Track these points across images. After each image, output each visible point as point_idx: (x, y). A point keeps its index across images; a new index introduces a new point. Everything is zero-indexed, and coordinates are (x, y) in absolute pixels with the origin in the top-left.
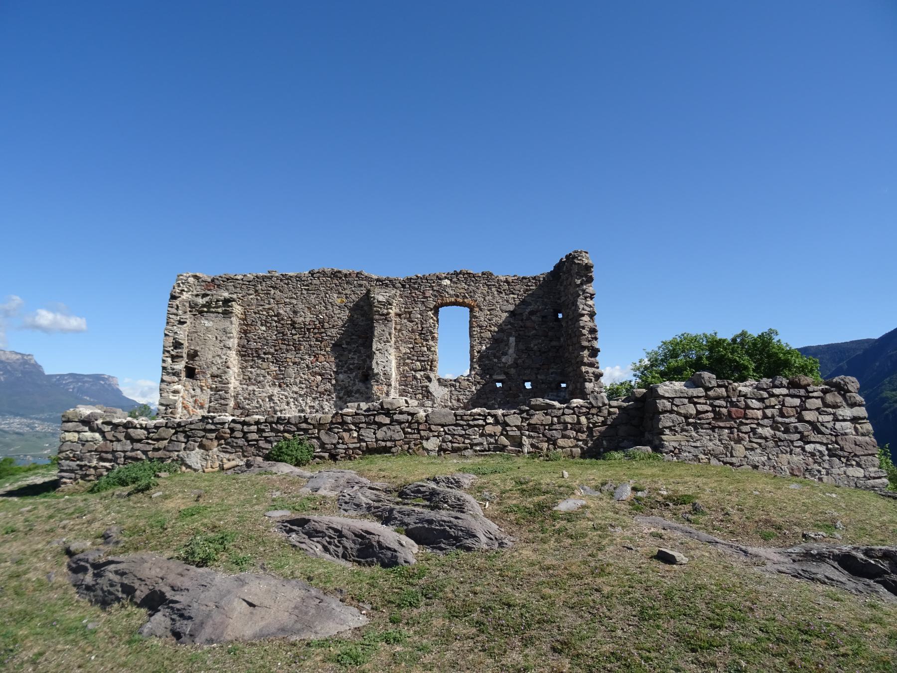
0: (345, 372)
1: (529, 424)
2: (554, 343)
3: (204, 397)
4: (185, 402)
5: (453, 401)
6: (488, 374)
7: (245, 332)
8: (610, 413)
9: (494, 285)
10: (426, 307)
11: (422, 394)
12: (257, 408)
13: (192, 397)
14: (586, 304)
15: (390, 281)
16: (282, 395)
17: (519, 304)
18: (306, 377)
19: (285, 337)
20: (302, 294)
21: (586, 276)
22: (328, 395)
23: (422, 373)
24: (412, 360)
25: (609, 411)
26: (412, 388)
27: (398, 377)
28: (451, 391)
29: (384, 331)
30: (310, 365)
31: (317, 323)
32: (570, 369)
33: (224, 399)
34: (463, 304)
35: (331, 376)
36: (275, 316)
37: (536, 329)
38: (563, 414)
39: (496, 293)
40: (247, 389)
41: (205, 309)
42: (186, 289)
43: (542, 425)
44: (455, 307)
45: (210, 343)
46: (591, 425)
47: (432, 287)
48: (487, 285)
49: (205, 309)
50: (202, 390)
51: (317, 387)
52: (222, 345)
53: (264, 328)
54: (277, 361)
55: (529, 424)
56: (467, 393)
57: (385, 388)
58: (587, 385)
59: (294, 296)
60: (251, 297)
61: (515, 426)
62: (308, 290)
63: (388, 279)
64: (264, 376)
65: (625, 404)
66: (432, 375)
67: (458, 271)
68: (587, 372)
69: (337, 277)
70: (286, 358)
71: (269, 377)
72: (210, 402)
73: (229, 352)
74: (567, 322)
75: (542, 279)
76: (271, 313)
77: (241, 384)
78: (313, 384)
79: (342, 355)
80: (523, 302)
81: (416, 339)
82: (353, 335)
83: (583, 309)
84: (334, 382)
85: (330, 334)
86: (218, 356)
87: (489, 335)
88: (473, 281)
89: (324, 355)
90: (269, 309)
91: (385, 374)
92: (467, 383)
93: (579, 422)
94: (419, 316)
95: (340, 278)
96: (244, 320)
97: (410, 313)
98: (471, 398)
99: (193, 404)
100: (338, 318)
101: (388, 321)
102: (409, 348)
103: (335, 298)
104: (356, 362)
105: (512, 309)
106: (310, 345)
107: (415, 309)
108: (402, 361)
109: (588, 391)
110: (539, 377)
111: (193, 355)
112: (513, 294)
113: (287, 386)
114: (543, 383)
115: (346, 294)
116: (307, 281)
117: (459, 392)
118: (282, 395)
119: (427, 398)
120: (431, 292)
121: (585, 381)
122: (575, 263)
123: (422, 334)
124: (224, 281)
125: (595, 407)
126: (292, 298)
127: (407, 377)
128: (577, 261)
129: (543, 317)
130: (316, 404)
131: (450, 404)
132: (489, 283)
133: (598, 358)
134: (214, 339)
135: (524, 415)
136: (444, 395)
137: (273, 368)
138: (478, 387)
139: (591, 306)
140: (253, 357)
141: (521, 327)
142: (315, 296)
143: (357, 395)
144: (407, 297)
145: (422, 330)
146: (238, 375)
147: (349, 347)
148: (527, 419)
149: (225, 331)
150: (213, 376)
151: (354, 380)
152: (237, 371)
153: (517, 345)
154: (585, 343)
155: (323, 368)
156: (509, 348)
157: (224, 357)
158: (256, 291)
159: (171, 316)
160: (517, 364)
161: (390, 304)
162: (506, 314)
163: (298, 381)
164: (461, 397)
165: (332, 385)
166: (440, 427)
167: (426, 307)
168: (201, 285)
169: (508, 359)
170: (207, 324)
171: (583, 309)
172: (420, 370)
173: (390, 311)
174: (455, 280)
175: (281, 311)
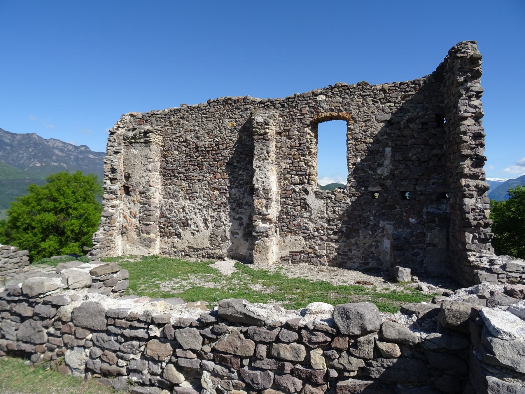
0: (237, 187)
1: (213, 350)
2: (435, 152)
3: (136, 209)
4: (125, 213)
5: (329, 213)
6: (363, 186)
7: (165, 157)
8: (378, 353)
9: (369, 95)
10: (303, 124)
11: (300, 206)
12: (175, 217)
13: (129, 209)
14: (469, 105)
15: (271, 102)
16: (191, 206)
17: (396, 113)
18: (207, 191)
19: (192, 159)
20: (202, 121)
21: (472, 71)
22: (224, 207)
23: (300, 186)
24: (292, 174)
25: (376, 348)
26: (292, 200)
27: (280, 191)
28: (327, 203)
29: (262, 149)
30: (210, 182)
31: (214, 145)
32: (451, 180)
33: (148, 211)
34: (338, 118)
35: (226, 191)
36: (184, 142)
37: (414, 138)
38: (278, 340)
39: (371, 103)
40: (168, 202)
41: (133, 141)
42: (121, 126)
43: (236, 356)
44: (330, 122)
45: (137, 167)
46: (334, 374)
47: (308, 104)
48: (362, 96)
49: (133, 141)
50: (134, 204)
51: (216, 200)
52: (145, 168)
53: (177, 153)
54: (187, 179)
55: (213, 350)
56: (342, 205)
57: (264, 202)
58: (467, 201)
59: (197, 124)
60: (168, 127)
61: (192, 350)
62: (206, 117)
63: (269, 101)
64: (179, 192)
65: (418, 336)
66: (309, 188)
67: (333, 86)
68: (468, 186)
69: (227, 103)
70: (193, 176)
71: (182, 192)
72: (140, 213)
73: (150, 173)
74: (449, 128)
75: (422, 82)
76: (182, 140)
77: (164, 198)
78: (213, 197)
79: (234, 172)
80: (401, 110)
81: (294, 155)
82: (242, 154)
83: (466, 111)
84: (228, 195)
85: (223, 154)
86: (143, 177)
87: (364, 147)
88: (347, 93)
89: (220, 173)
90: (180, 136)
91: (264, 189)
92: (342, 195)
93: (307, 362)
94: (297, 133)
95: (231, 104)
96: (164, 146)
97: (289, 130)
98: (347, 210)
99: (129, 214)
100: (230, 140)
101: (266, 140)
102: (289, 164)
103: (228, 123)
104: (245, 178)
105: (388, 118)
106: (210, 165)
107: (293, 126)
108: (282, 176)
109: (466, 209)
110: (418, 188)
111: (128, 177)
112: (390, 102)
113: (195, 199)
114: (422, 194)
115: (235, 118)
116: (206, 110)
117: (335, 204)
118: (191, 206)
119: (306, 210)
120: (307, 109)
121: (464, 196)
122: (458, 58)
123: (299, 149)
124: (149, 117)
125: (344, 336)
126: (195, 126)
127: (287, 190)
128: (459, 55)
129: (423, 124)
130: (215, 214)
131: (326, 215)
132: (364, 94)
133: (484, 169)
134: (140, 164)
135: (207, 331)
136: (320, 207)
137: (184, 185)
138: (354, 199)
139: (476, 107)
140: (171, 176)
141: (399, 136)
142: (212, 122)
143: (246, 207)
144: (286, 116)
145: (300, 146)
146: (162, 191)
147: (239, 165)
148: (211, 340)
149: (147, 157)
150: (141, 193)
151: (244, 194)
152: (160, 188)
153: (393, 156)
154: (466, 152)
155: (220, 184)
156: (385, 160)
157: (147, 178)
158: (171, 122)
159: (109, 148)
160: (393, 175)
161: (267, 124)
162: (382, 124)
163: (202, 195)
164: (336, 209)
165: (227, 198)
166: (88, 332)
167: (303, 124)
168: (135, 122)
169: (383, 171)
170: (136, 152)
171: (466, 111)
172: (299, 184)
173: (267, 130)
174: (330, 94)
175: (188, 138)
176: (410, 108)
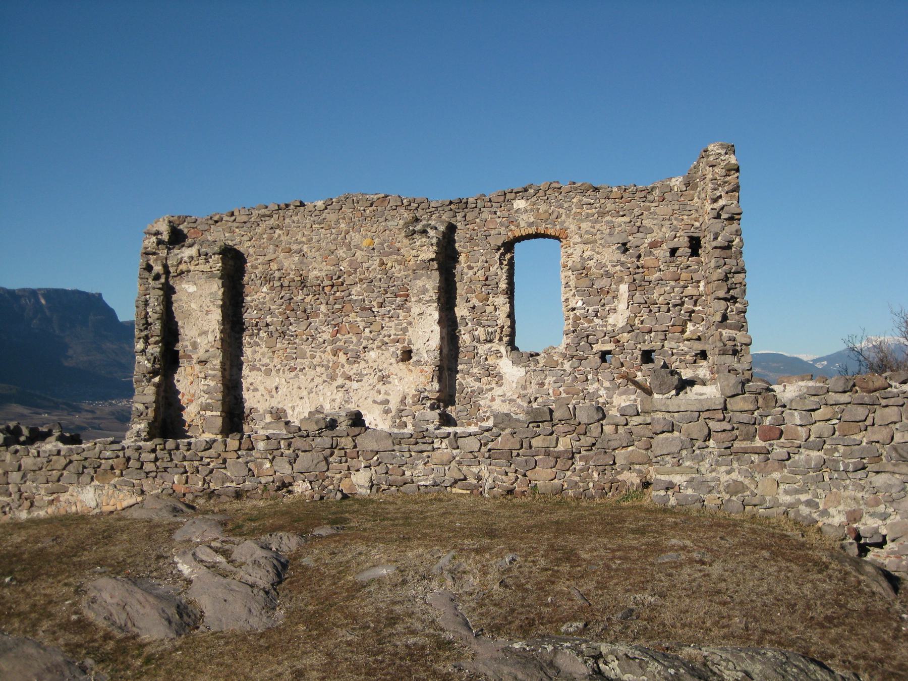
176: (653, 227)
